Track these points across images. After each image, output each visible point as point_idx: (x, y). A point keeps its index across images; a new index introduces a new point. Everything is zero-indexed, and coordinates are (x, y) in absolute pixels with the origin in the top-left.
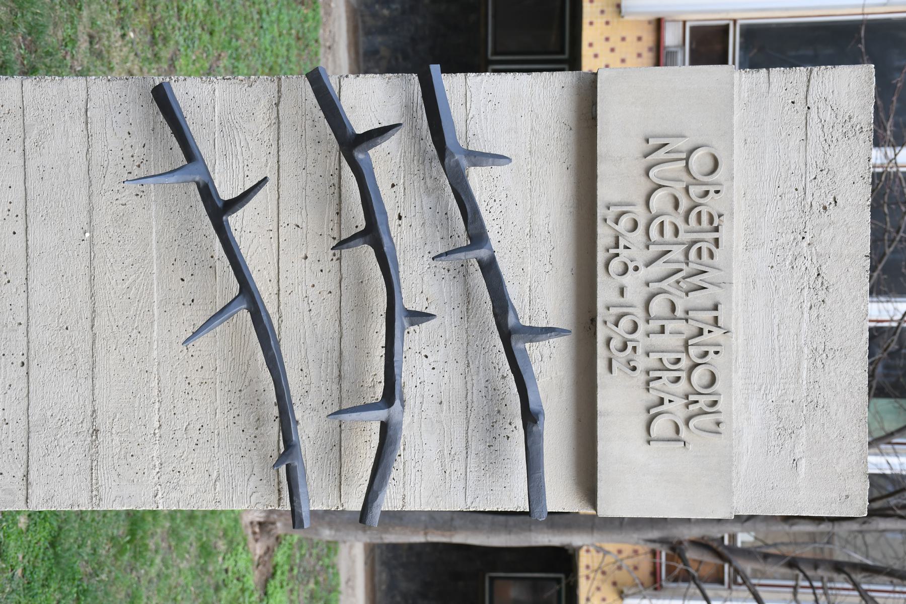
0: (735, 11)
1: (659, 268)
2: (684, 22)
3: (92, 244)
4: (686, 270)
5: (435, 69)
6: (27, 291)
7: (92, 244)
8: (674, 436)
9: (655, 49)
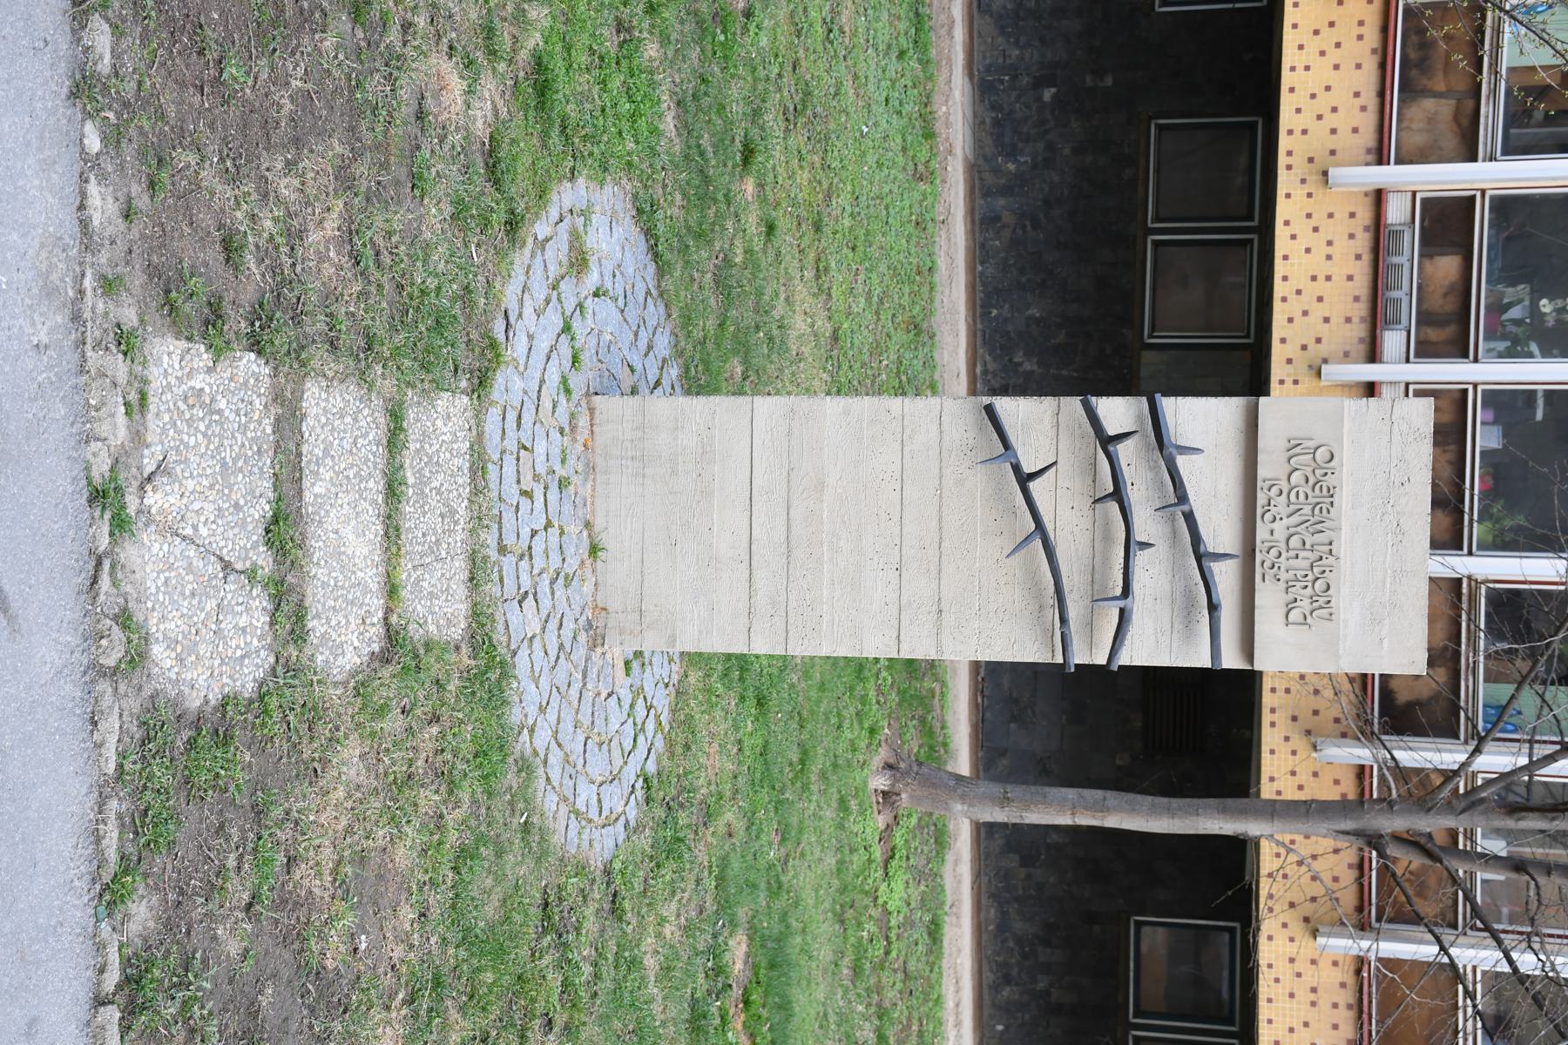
0: (1483, 181)
1: (1296, 519)
2: (1414, 193)
3: (941, 497)
5: (1158, 396)
7: (941, 497)
8: (1302, 620)
9: (1372, 229)
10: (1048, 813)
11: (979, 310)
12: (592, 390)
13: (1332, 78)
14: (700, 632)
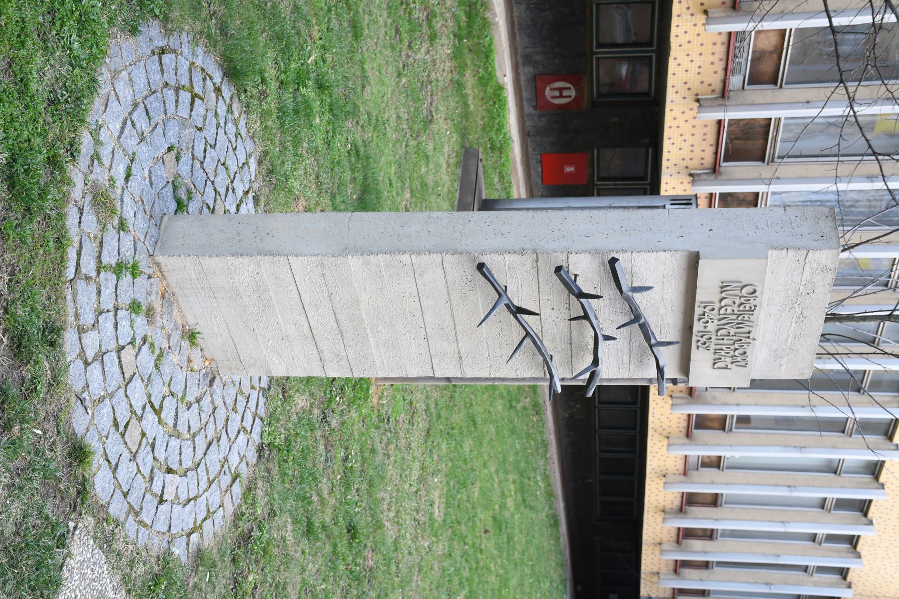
4: (736, 321)
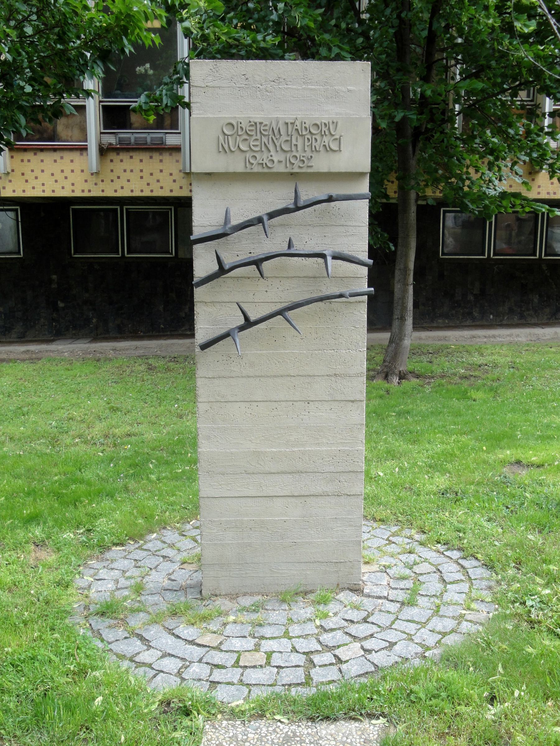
1: (271, 147)
2: (101, 133)
5: (192, 238)
6: (280, 401)
10: (408, 298)
11: (161, 334)
12: (199, 596)
13: (47, 173)
14: (351, 526)
